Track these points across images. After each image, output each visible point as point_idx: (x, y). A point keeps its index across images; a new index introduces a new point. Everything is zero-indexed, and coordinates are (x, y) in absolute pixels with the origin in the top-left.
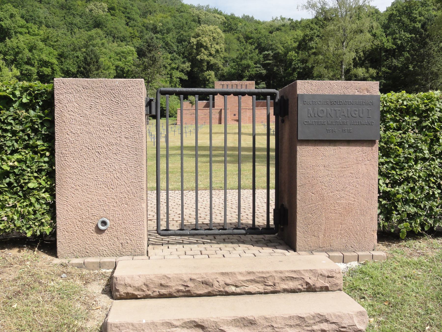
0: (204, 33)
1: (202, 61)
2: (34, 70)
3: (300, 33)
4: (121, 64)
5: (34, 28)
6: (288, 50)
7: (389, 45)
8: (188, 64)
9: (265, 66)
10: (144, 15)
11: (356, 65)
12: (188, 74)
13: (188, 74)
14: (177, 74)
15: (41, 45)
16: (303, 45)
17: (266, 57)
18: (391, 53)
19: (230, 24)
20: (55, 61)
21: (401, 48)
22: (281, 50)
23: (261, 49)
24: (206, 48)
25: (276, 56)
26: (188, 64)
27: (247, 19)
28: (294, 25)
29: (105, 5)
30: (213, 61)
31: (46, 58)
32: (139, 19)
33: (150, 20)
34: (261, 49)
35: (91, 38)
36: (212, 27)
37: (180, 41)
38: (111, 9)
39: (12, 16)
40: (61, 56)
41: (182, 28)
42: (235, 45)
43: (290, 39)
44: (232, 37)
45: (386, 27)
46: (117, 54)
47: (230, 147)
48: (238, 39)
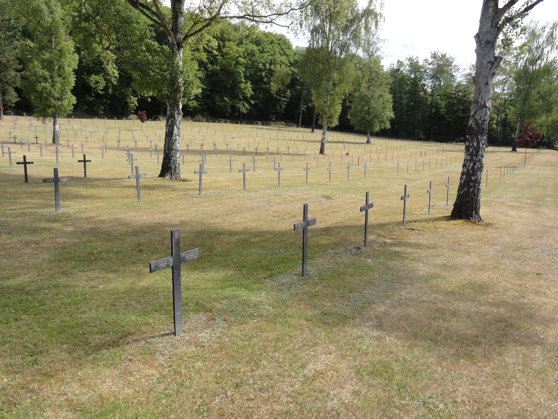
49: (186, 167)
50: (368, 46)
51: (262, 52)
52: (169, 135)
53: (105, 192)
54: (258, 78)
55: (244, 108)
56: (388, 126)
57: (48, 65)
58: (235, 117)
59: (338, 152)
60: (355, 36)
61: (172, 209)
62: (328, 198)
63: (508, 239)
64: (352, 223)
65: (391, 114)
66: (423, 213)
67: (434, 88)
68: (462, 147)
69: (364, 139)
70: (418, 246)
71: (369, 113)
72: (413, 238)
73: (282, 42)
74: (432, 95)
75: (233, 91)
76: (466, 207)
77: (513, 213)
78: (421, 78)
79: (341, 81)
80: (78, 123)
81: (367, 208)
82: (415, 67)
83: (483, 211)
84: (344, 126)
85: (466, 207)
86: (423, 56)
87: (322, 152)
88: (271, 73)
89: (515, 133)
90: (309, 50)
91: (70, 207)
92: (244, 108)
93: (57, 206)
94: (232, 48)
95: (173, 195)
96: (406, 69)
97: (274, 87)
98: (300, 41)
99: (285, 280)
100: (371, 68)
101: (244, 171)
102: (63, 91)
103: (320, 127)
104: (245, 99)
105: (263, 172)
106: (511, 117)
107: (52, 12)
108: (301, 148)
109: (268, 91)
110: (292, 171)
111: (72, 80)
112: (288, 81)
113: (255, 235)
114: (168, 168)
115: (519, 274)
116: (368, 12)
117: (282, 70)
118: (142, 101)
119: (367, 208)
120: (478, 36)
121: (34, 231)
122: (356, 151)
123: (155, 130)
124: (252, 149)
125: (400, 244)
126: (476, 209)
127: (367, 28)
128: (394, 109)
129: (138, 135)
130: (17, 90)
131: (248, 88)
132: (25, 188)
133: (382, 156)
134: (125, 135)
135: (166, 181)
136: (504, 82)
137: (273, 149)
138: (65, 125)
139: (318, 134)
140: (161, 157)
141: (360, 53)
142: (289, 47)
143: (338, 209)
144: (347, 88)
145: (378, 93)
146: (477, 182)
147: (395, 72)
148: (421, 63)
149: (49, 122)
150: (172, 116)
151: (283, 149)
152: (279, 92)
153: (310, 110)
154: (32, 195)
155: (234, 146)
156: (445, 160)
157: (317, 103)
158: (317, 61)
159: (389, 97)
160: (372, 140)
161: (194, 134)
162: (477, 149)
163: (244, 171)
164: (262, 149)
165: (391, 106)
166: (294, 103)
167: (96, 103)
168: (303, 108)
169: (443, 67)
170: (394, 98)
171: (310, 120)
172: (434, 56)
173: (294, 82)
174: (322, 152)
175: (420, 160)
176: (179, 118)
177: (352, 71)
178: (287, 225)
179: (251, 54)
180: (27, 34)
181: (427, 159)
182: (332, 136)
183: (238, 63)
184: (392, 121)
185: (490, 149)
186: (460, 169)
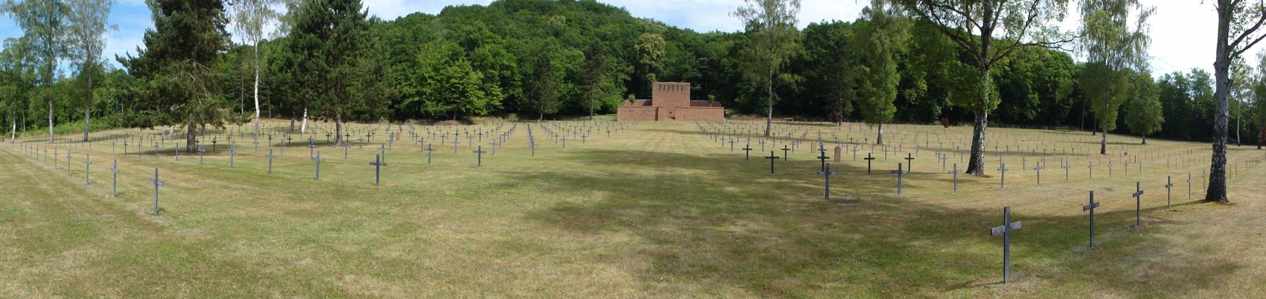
0: (647, 40)
1: (645, 64)
2: (496, 73)
3: (731, 43)
4: (569, 66)
5: (499, 38)
6: (721, 57)
7: (807, 57)
8: (632, 67)
9: (701, 70)
10: (597, 25)
11: (781, 71)
12: (633, 76)
13: (633, 76)
14: (623, 76)
15: (503, 52)
16: (733, 52)
17: (702, 63)
18: (808, 65)
19: (672, 34)
20: (514, 65)
21: (816, 62)
22: (715, 57)
23: (698, 55)
24: (649, 53)
25: (711, 63)
26: (632, 67)
27: (688, 31)
28: (726, 37)
29: (564, 18)
30: (654, 64)
31: (505, 62)
32: (593, 29)
33: (603, 29)
34: (698, 55)
35: (547, 44)
36: (654, 36)
37: (625, 47)
38: (568, 21)
39: (480, 29)
40: (521, 61)
41: (627, 36)
42: (676, 52)
43: (723, 47)
44: (673, 45)
45: (805, 43)
46: (568, 57)
47: (661, 154)
48: (678, 46)
49: (989, 165)
50: (1140, 62)
51: (1047, 66)
52: (976, 139)
53: (928, 183)
54: (1045, 88)
55: (1031, 115)
56: (1160, 129)
57: (877, 84)
58: (1021, 122)
59: (1117, 152)
60: (1128, 54)
61: (978, 197)
62: (1109, 190)
63: (1244, 213)
64: (1128, 208)
65: (1162, 119)
66: (1186, 199)
67: (1196, 98)
68: (1210, 146)
69: (1140, 141)
70: (1180, 223)
71: (1142, 118)
72: (1175, 218)
73: (1065, 59)
74: (1195, 102)
75: (1022, 100)
76: (1216, 192)
77: (1252, 195)
78: (1186, 89)
79: (1117, 91)
80: (894, 128)
81: (1138, 194)
82: (1179, 79)
83: (1229, 195)
84: (1122, 130)
85: (1216, 192)
86: (1186, 71)
87: (1103, 152)
88: (1056, 85)
89: (1252, 137)
90: (1089, 65)
91: (906, 193)
92: (1031, 115)
93: (899, 192)
94: (1022, 64)
95: (980, 188)
96: (1173, 81)
97: (1059, 96)
98: (1081, 57)
99: (1078, 249)
100: (1143, 80)
101: (1037, 169)
102: (886, 103)
103: (1101, 131)
104: (1033, 107)
105: (1052, 170)
106: (1257, 122)
107: (883, 44)
108: (1084, 149)
109: (1053, 100)
110: (1078, 169)
111: (894, 94)
112: (1070, 92)
113: (1051, 219)
114: (974, 166)
115: (1247, 235)
116: (1138, 35)
117: (1065, 82)
118: (945, 110)
119: (1138, 194)
120: (1215, 64)
121: (888, 208)
122: (1132, 151)
123: (962, 135)
124: (1040, 150)
125: (1166, 222)
126: (1224, 194)
127: (1137, 48)
128: (1164, 115)
129: (942, 138)
130: (853, 103)
131: (1035, 98)
132: (867, 177)
133: (1155, 155)
134: (931, 138)
135: (972, 177)
136: (1248, 94)
137: (1059, 150)
138: (888, 130)
139: (1099, 137)
140: (969, 156)
141: (1133, 67)
142: (1071, 62)
143: (1116, 199)
144: (1123, 97)
145: (1150, 100)
146: (1223, 172)
147: (1164, 83)
148: (1184, 76)
149: (875, 128)
150: (979, 124)
151: (1068, 150)
152: (1063, 101)
153: (1091, 115)
154: (875, 182)
155: (1024, 148)
156: (1197, 156)
157: (1096, 109)
158: (1094, 71)
159: (1158, 104)
160: (1147, 141)
161: (995, 137)
162: (1221, 147)
163: (1037, 169)
164: (1050, 150)
165: (1160, 112)
166: (1076, 110)
167: (913, 112)
168: (1085, 114)
169: (1201, 80)
170: (1164, 105)
171: (1091, 124)
172: (1195, 71)
173: (1076, 92)
174: (1103, 152)
175: (1186, 158)
176: (984, 126)
177: (1127, 85)
178: (1078, 211)
179: (1038, 69)
180: (864, 61)
181: (1192, 157)
182: (1111, 138)
183: (1026, 77)
184: (1163, 125)
185: (1229, 146)
186: (1210, 163)
